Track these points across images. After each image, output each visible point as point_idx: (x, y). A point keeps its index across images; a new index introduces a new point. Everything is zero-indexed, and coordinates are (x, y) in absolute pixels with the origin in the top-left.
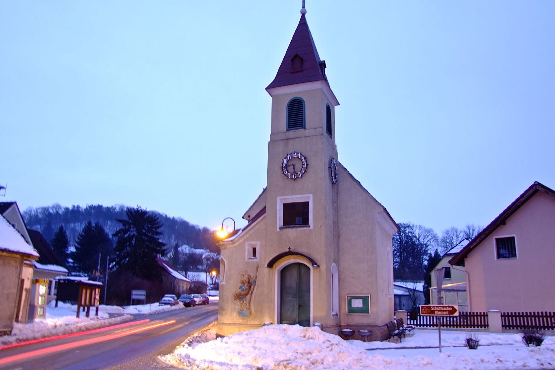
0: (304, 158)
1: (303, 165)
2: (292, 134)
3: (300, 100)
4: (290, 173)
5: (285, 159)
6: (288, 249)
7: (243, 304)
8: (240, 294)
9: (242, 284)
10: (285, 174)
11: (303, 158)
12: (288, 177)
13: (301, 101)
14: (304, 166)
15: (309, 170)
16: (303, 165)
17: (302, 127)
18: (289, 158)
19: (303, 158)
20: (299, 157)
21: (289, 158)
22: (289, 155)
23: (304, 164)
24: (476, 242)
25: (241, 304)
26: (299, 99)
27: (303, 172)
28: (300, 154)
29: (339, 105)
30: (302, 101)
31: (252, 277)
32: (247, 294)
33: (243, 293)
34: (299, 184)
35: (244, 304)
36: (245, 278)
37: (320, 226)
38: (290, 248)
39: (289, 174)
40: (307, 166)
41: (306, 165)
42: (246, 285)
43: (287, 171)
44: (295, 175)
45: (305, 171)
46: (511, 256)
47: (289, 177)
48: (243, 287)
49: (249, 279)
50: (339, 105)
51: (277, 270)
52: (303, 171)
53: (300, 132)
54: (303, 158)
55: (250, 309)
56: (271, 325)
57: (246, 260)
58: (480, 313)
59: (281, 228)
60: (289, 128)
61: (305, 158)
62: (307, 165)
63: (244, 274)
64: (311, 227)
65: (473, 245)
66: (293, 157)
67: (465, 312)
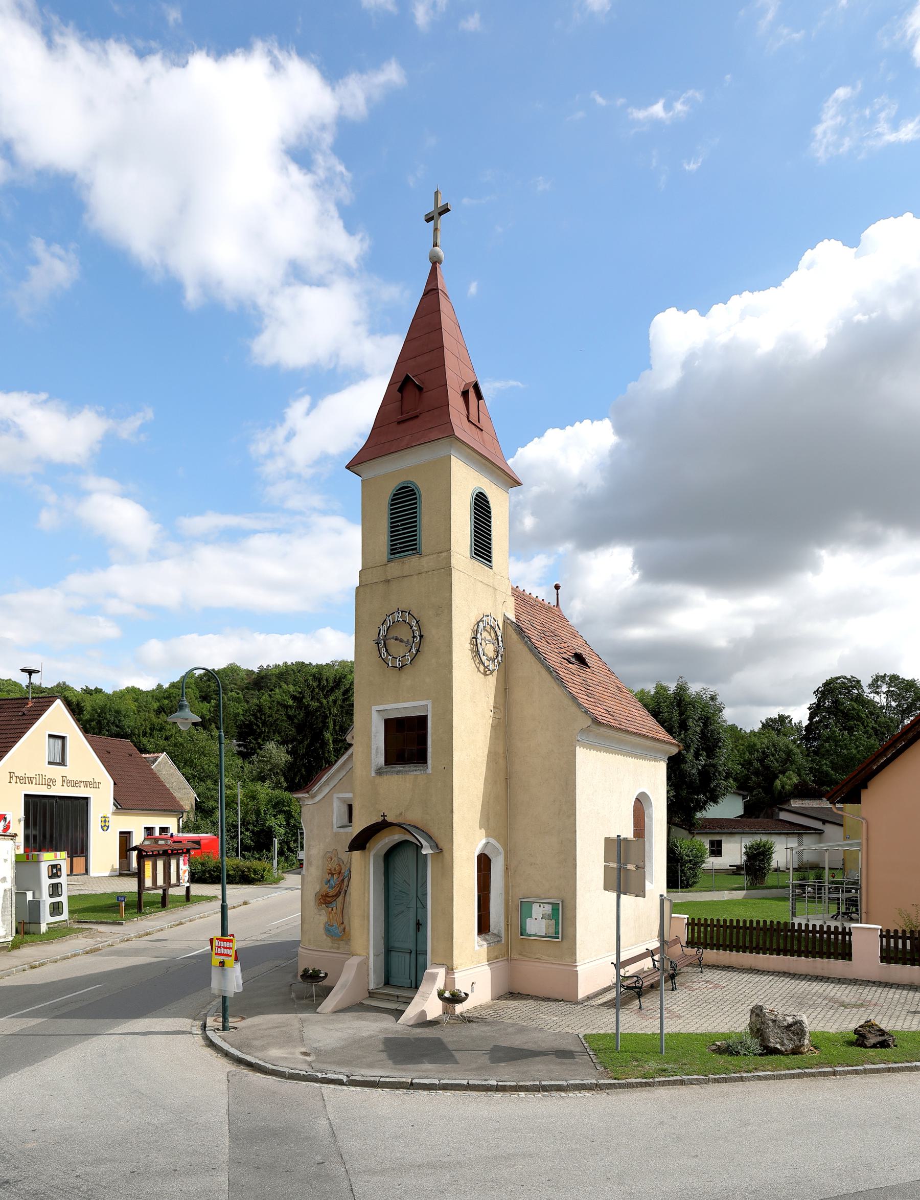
0: (415, 622)
1: (414, 637)
2: (395, 569)
3: (413, 487)
4: (391, 656)
5: (382, 625)
6: (382, 816)
7: (332, 913)
8: (327, 896)
9: (330, 875)
10: (382, 658)
11: (414, 623)
12: (388, 664)
13: (413, 490)
14: (415, 639)
15: (425, 648)
16: (414, 637)
17: (414, 552)
18: (390, 624)
19: (414, 623)
20: (407, 621)
21: (390, 624)
22: (389, 616)
23: (415, 635)
24: (885, 756)
25: (330, 913)
26: (409, 485)
27: (414, 653)
28: (409, 613)
29: (519, 484)
30: (416, 490)
31: (345, 863)
32: (338, 895)
33: (332, 892)
34: (407, 679)
35: (334, 914)
36: (334, 865)
37: (444, 768)
38: (384, 816)
39: (389, 657)
40: (420, 639)
41: (418, 638)
42: (335, 877)
43: (387, 651)
44: (399, 661)
45: (418, 651)
46: (766, 817)
47: (390, 665)
48: (332, 882)
49: (339, 865)
50: (519, 484)
51: (372, 853)
52: (414, 651)
53: (412, 562)
54: (414, 622)
55: (343, 923)
56: (225, 970)
57: (335, 829)
58: (706, 920)
59: (379, 772)
60: (392, 554)
61: (417, 622)
62: (421, 636)
63: (333, 856)
64: (429, 771)
65: (879, 761)
66: (396, 621)
67: (722, 919)
